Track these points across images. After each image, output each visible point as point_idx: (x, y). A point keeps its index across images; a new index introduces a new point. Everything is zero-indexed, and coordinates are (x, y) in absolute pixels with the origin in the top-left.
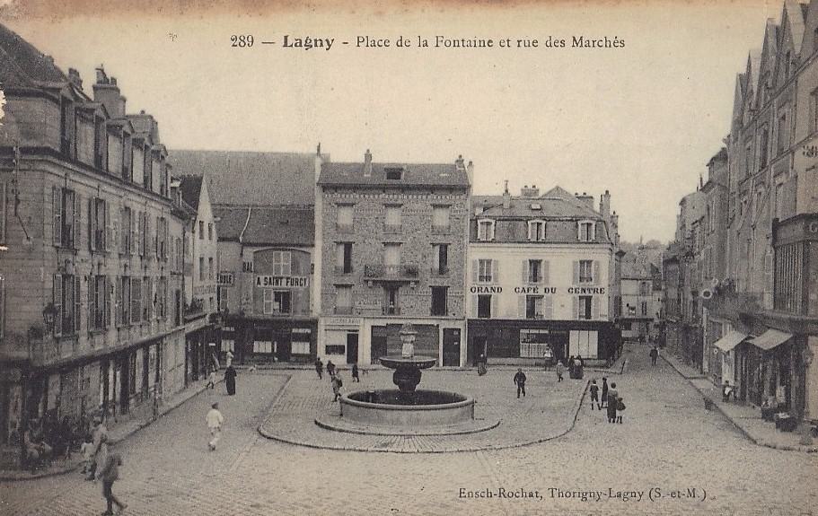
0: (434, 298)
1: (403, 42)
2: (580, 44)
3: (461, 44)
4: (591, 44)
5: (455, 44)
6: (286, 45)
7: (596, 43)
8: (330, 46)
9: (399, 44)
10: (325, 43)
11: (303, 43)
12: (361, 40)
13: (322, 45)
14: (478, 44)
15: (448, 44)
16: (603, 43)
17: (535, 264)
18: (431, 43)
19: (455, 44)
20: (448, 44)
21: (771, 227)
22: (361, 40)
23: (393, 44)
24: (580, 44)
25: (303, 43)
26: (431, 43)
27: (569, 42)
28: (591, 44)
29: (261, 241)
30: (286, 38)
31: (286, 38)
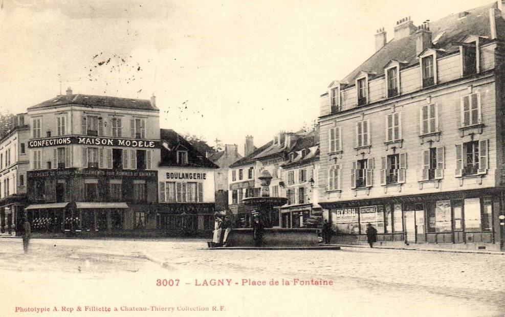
4: (133, 309)
6: (196, 285)
18: (83, 309)
26: (83, 309)
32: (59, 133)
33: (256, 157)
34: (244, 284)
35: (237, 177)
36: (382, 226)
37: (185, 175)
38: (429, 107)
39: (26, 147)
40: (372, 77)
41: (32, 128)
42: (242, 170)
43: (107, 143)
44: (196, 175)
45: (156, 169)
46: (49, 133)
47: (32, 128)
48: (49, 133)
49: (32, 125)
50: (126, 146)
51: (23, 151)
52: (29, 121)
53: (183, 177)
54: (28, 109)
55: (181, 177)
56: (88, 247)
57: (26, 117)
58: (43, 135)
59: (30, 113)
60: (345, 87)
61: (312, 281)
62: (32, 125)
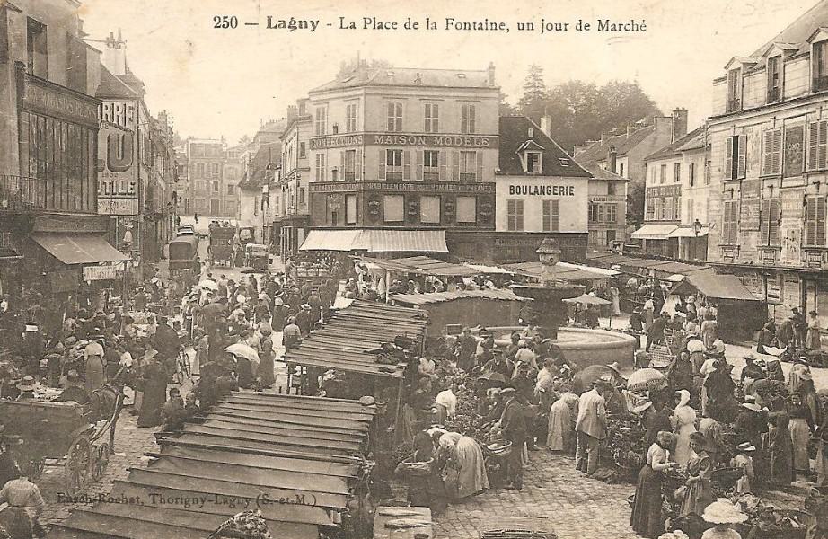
0: (558, 226)
1: (412, 25)
2: (605, 28)
3: (472, 27)
4: (617, 28)
5: (466, 26)
6: (269, 26)
7: (622, 27)
8: (314, 27)
9: (579, 27)
10: (310, 25)
11: (287, 25)
12: (368, 21)
13: (306, 27)
14: (526, 27)
15: (459, 26)
16: (630, 27)
17: (662, 183)
19: (466, 26)
20: (459, 26)
21: (11, 39)
22: (368, 21)
23: (400, 26)
24: (605, 28)
25: (287, 25)
27: (423, 24)
28: (617, 28)
29: (125, 147)
30: (269, 20)
31: (269, 20)
32: (348, 129)
33: (682, 148)
34: (367, 26)
35: (658, 179)
36: (509, 229)
37: (539, 188)
38: (819, 126)
39: (307, 147)
40: (792, 54)
41: (315, 121)
42: (679, 164)
43: (417, 142)
44: (558, 189)
45: (492, 180)
46: (336, 127)
47: (315, 121)
48: (336, 127)
49: (314, 115)
50: (445, 146)
51: (303, 154)
52: (311, 109)
53: (536, 192)
54: (310, 92)
55: (533, 191)
56: (693, 143)
57: (308, 105)
58: (329, 130)
59: (312, 99)
60: (751, 68)
61: (475, 23)
62: (314, 115)
